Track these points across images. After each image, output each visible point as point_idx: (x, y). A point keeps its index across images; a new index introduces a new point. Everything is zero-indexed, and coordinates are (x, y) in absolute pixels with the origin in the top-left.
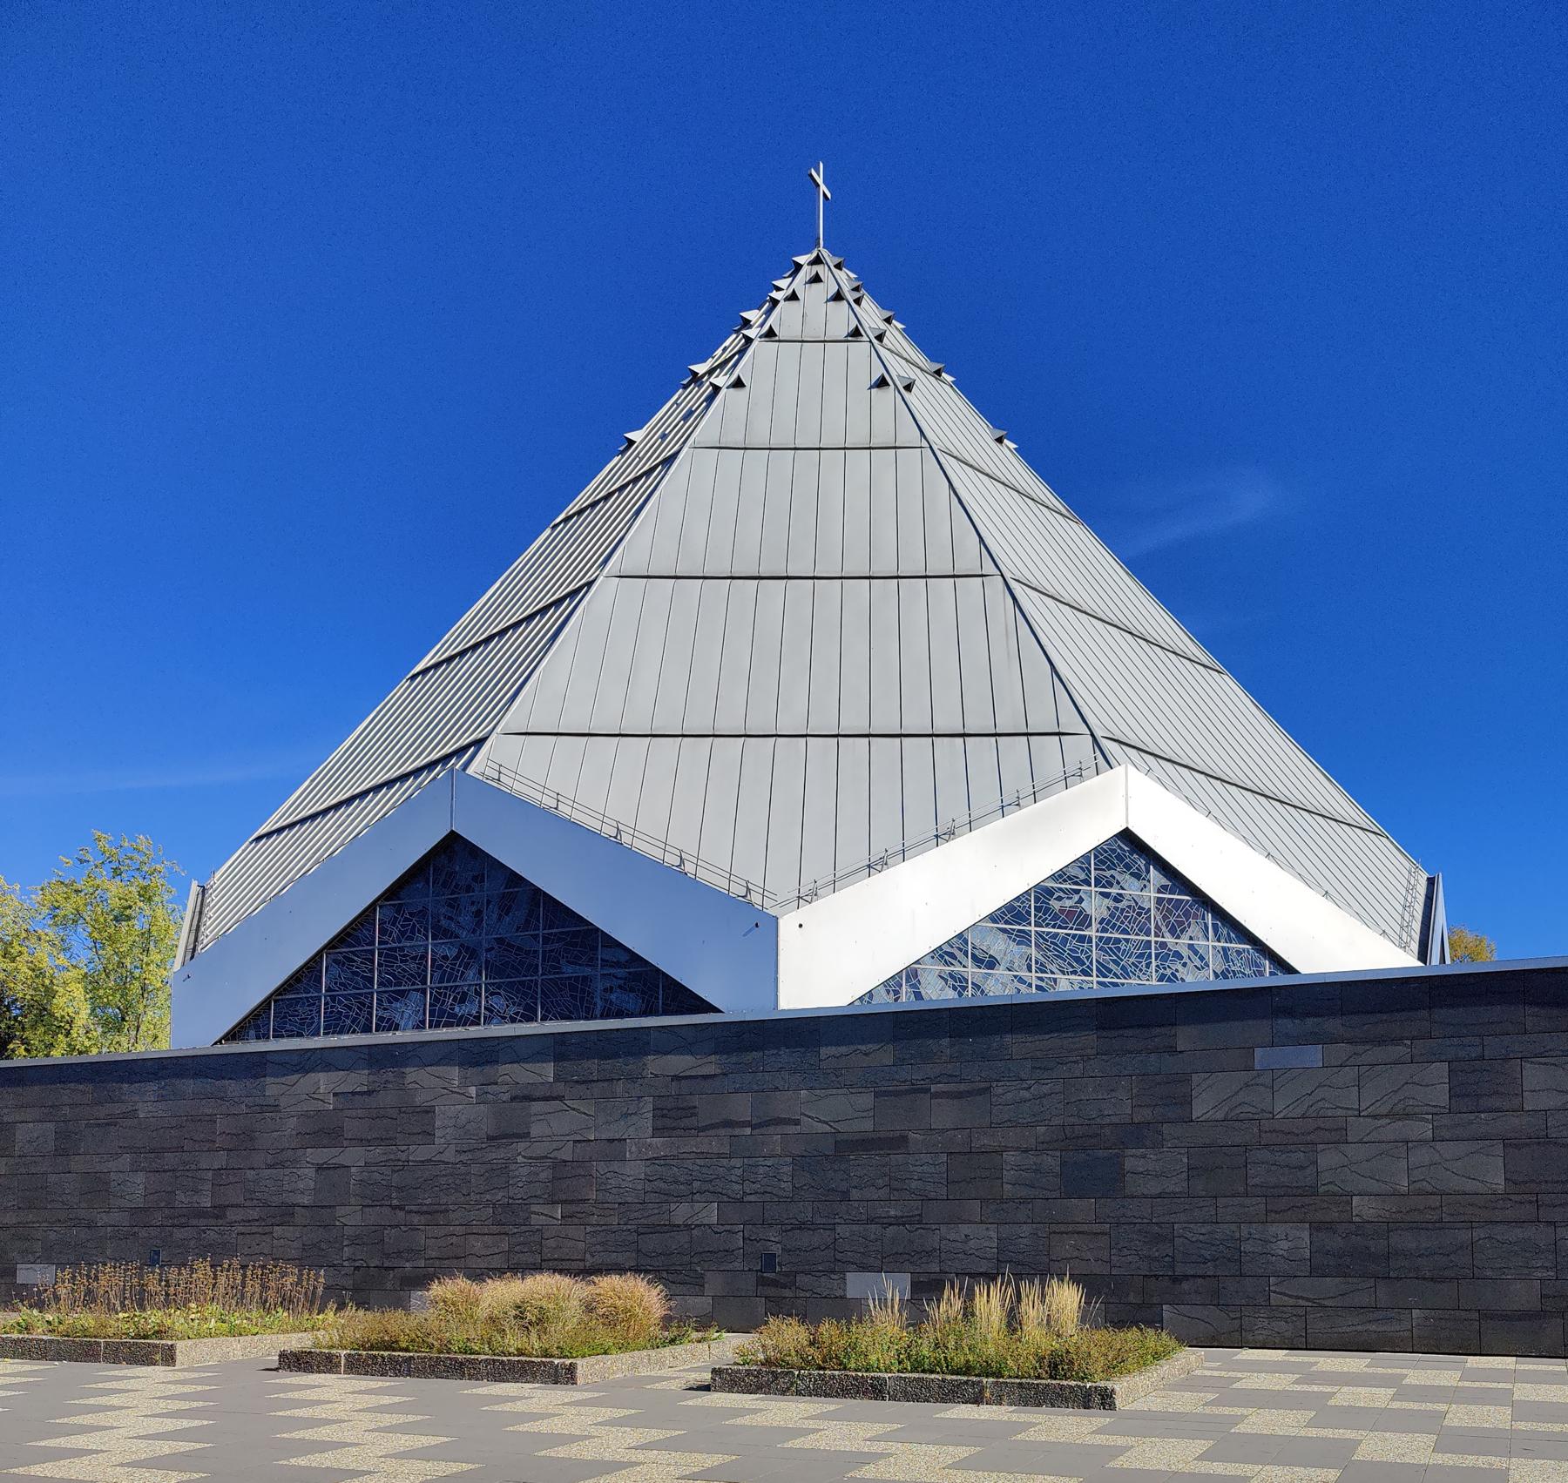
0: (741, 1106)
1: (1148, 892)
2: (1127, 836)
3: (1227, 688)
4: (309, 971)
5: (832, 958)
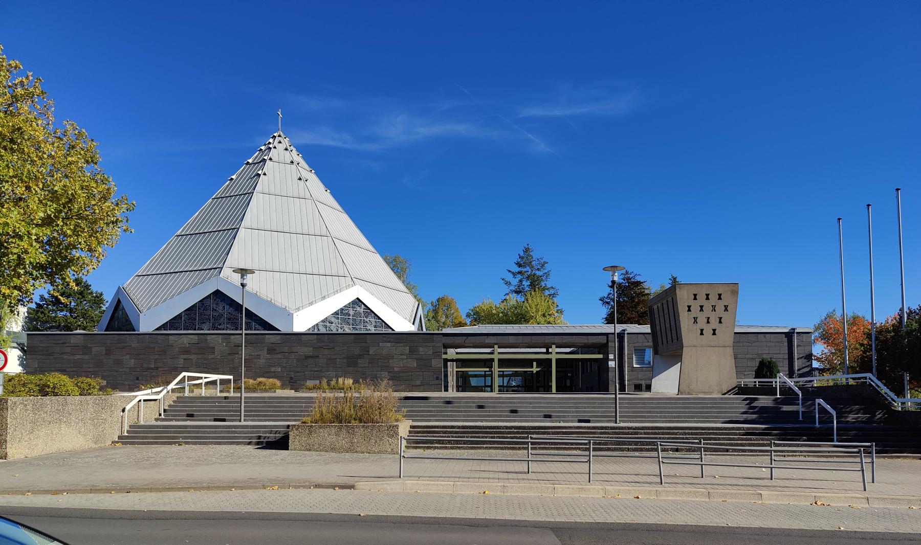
0: (286, 349)
1: (361, 310)
2: (358, 299)
3: (345, 218)
4: (179, 316)
5: (302, 322)
